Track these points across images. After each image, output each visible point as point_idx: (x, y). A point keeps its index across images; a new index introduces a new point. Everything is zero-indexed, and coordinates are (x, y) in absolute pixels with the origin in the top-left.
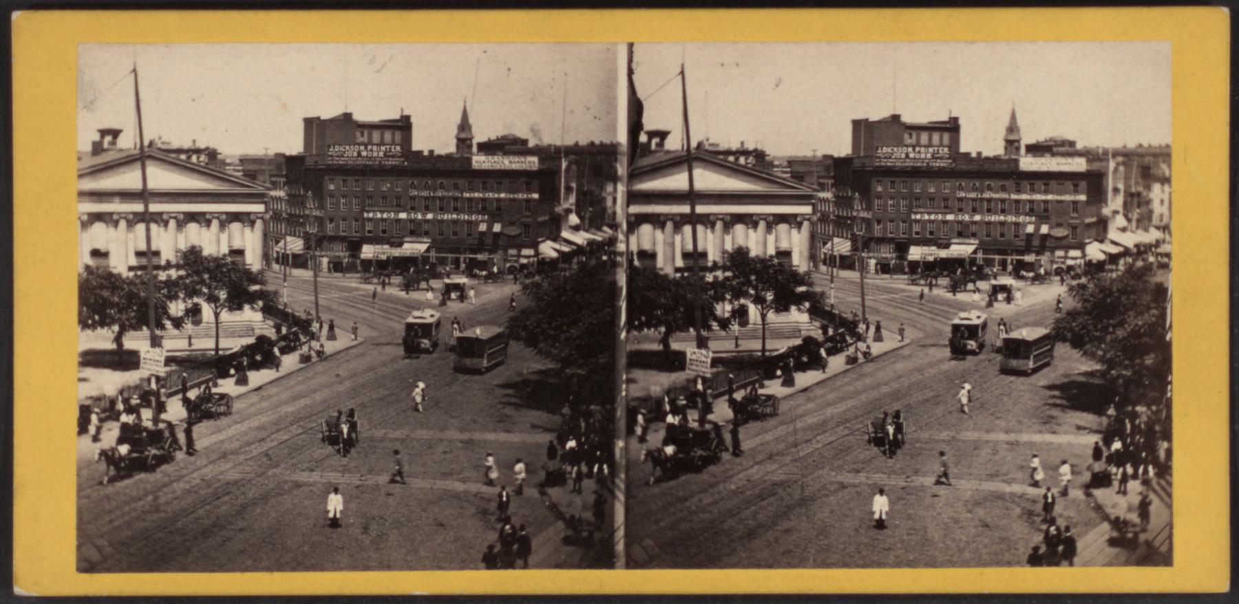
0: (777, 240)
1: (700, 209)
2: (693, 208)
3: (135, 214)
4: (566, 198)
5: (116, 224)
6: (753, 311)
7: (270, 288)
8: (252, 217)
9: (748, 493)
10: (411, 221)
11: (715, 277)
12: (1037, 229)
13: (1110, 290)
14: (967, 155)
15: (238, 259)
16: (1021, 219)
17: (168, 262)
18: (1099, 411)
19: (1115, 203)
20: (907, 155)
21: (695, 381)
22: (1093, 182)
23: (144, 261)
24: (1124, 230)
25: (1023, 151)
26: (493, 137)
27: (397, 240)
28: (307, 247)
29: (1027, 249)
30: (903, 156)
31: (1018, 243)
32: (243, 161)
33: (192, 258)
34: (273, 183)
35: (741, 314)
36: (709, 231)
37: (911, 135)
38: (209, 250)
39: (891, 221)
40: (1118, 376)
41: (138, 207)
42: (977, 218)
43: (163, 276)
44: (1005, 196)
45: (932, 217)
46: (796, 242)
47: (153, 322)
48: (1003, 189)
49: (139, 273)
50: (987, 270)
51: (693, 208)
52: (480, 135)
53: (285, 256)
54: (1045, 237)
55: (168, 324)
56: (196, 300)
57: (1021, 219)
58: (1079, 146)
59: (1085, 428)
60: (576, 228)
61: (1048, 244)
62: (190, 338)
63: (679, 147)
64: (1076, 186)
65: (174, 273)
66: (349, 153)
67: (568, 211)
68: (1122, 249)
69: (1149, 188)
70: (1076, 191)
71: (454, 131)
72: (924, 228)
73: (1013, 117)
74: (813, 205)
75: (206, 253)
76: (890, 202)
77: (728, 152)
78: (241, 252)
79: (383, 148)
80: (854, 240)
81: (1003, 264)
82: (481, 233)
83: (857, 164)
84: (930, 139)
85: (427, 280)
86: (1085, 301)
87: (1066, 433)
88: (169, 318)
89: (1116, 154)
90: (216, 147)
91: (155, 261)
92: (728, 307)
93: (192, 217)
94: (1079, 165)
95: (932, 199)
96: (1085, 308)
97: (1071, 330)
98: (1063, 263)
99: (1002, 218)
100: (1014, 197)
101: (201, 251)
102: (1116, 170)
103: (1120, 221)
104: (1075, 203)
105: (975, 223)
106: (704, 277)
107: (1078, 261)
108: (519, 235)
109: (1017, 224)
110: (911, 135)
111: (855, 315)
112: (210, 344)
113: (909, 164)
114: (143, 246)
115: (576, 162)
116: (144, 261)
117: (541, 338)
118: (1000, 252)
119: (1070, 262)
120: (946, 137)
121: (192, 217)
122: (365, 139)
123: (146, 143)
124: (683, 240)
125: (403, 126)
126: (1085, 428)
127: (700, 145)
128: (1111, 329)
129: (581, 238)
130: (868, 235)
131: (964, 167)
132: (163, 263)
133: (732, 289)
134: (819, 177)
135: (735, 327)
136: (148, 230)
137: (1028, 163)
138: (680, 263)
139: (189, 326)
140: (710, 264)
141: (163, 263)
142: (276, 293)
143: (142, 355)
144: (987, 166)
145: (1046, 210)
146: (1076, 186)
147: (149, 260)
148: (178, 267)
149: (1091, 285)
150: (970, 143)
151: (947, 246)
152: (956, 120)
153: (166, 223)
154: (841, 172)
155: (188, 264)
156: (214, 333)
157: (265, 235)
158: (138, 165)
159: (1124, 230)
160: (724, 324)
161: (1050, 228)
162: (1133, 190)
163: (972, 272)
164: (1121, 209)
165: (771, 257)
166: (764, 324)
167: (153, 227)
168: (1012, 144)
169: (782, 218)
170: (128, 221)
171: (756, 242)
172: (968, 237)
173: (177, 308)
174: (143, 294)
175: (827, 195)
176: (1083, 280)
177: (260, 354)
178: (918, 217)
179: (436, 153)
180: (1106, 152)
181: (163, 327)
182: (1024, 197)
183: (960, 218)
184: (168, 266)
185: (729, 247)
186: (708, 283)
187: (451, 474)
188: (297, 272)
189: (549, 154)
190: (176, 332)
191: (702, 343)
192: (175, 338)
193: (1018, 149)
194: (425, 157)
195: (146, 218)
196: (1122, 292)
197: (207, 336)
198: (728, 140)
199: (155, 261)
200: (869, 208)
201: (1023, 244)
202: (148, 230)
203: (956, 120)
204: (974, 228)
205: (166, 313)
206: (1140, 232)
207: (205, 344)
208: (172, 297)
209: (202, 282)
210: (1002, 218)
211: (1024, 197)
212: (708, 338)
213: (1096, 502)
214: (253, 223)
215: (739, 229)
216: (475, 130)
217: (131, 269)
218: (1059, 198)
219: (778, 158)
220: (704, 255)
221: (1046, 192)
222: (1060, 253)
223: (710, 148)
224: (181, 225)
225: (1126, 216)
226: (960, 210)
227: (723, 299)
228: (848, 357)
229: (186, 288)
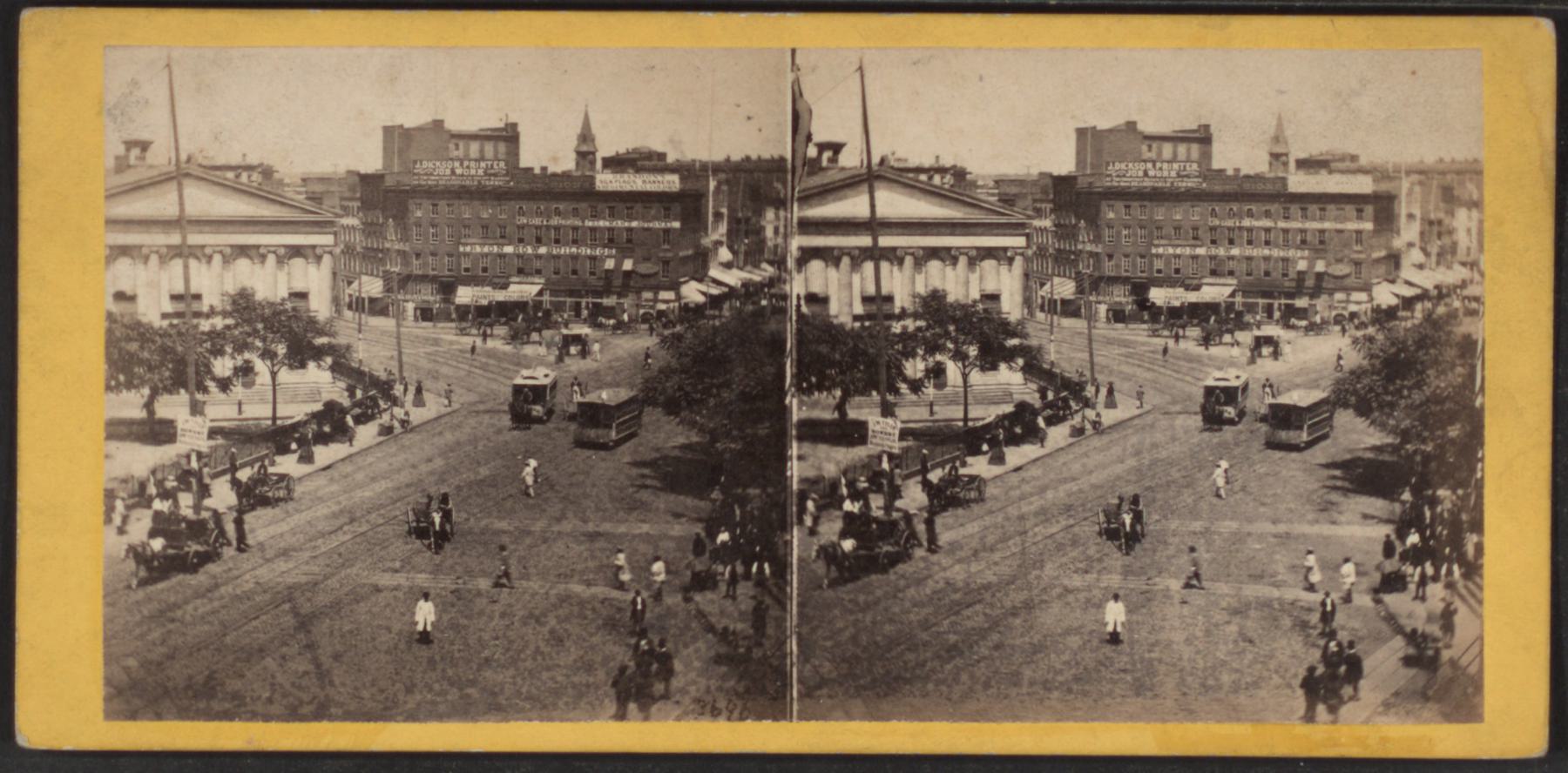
0: (981, 278)
1: (885, 241)
2: (875, 240)
3: (169, 247)
4: (715, 229)
5: (263, 257)
6: (953, 370)
7: (341, 340)
8: (318, 251)
9: (258, 599)
10: (519, 256)
11: (905, 328)
12: (619, 264)
13: (1404, 342)
14: (1222, 171)
15: (300, 304)
16: (1291, 253)
17: (903, 309)
18: (701, 494)
19: (1409, 232)
20: (1146, 174)
21: (879, 458)
22: (1382, 207)
23: (181, 307)
24: (1421, 267)
25: (599, 164)
26: (622, 150)
27: (503, 281)
28: (1080, 290)
29: (607, 291)
30: (1141, 173)
31: (1287, 284)
32: (998, 183)
33: (933, 305)
34: (344, 208)
35: (937, 372)
36: (895, 268)
37: (1150, 147)
38: (955, 293)
39: (1126, 256)
40: (1415, 452)
41: (865, 241)
42: (543, 250)
43: (205, 325)
44: (578, 223)
45: (1178, 251)
46: (1006, 284)
47: (192, 386)
48: (1267, 214)
49: (175, 321)
50: (1248, 318)
51: (875, 240)
52: (605, 149)
53: (360, 301)
54: (1320, 276)
55: (211, 385)
56: (939, 357)
57: (1291, 253)
58: (670, 159)
59: (1373, 517)
60: (728, 266)
61: (1324, 285)
62: (240, 404)
63: (166, 161)
64: (1360, 211)
65: (911, 325)
66: (1131, 174)
67: (718, 243)
68: (1418, 291)
69: (1451, 213)
70: (1360, 218)
71: (574, 143)
72: (1168, 263)
73: (1280, 126)
74: (1027, 236)
75: (951, 299)
76: (1125, 232)
77: (919, 170)
78: (995, 297)
79: (483, 164)
80: (1079, 278)
81: (1269, 311)
82: (1300, 273)
83: (389, 182)
85: (1231, 332)
86: (1372, 356)
87: (1349, 523)
88: (214, 379)
89: (717, 168)
90: (271, 163)
91: (195, 306)
92: (921, 366)
93: (934, 253)
94: (1363, 185)
95: (1177, 228)
96: (1373, 365)
97: (1355, 392)
98: (652, 307)
99: (1266, 252)
100: (1282, 224)
101: (945, 296)
102: (718, 189)
103: (1416, 255)
104: (1359, 232)
105: (539, 257)
106: (889, 328)
107: (1364, 306)
108: (656, 274)
109: (1285, 260)
110: (1150, 147)
111: (390, 373)
112: (958, 412)
113: (1148, 183)
114: (179, 288)
115: (727, 182)
116: (181, 307)
117: (1374, 405)
118: (1266, 295)
119: (662, 307)
120: (1195, 148)
121: (243, 251)
122: (1153, 155)
123: (876, 160)
124: (862, 279)
125: (509, 136)
126: (1373, 517)
127: (882, 161)
128: (1406, 392)
129: (733, 278)
130: (1096, 274)
131: (1218, 188)
132: (205, 309)
133: (925, 341)
134: (1035, 201)
135: (930, 391)
136: (186, 267)
137: (1299, 182)
138: (859, 309)
139: (238, 390)
140: (897, 311)
141: (205, 309)
142: (348, 347)
143: (180, 425)
144: (1247, 186)
145: (629, 241)
146: (1360, 211)
147: (189, 305)
148: (225, 314)
149: (1380, 337)
150: (531, 156)
151: (1197, 288)
152: (514, 126)
153: (901, 262)
154: (1070, 198)
155: (237, 311)
156: (270, 398)
157: (1026, 276)
158: (173, 185)
159: (1421, 267)
160: (916, 386)
161: (1328, 265)
162: (1432, 216)
163: (1227, 321)
164: (724, 239)
165: (975, 302)
166: (274, 385)
167: (193, 263)
168: (585, 156)
169: (989, 253)
170: (852, 258)
171: (958, 284)
172: (531, 274)
173: (223, 366)
174: (871, 351)
175: (1047, 223)
176: (1371, 330)
177: (332, 423)
178: (1161, 250)
179: (1243, 173)
180: (704, 167)
181: (205, 390)
182: (602, 223)
183: (1213, 251)
184: (213, 312)
185: (921, 289)
186: (895, 335)
187: (1262, 577)
188: (1067, 322)
189: (685, 170)
190: (222, 396)
191: (887, 410)
192: (222, 403)
193: (1286, 164)
194: (1228, 177)
195: (182, 252)
196: (1422, 343)
197: (951, 403)
198: (920, 156)
199: (195, 306)
200: (1098, 239)
201: (1294, 284)
202: (186, 267)
203: (514, 126)
204: (1232, 265)
205: (209, 371)
206: (749, 268)
207: (258, 411)
208: (219, 352)
209: (947, 334)
210: (1266, 252)
211: (602, 223)
212: (895, 405)
213: (1387, 610)
214: (319, 259)
215: (934, 265)
216: (598, 142)
217: (165, 316)
218: (1339, 226)
219: (984, 177)
220: (889, 299)
221: (631, 218)
222: (1339, 296)
223: (896, 165)
224: (227, 261)
225: (730, 248)
226: (521, 241)
227: (914, 355)
228: (1073, 427)
229: (925, 341)
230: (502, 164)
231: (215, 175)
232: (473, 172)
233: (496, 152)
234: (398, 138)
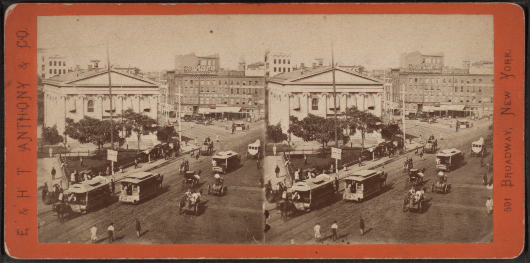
25: (246, 67)
30: (196, 70)
52: (248, 63)
84: (207, 63)
125: (215, 59)
178: (202, 95)
230: (214, 67)
231: (119, 71)
232: (204, 70)
233: (436, 61)
234: (180, 58)
